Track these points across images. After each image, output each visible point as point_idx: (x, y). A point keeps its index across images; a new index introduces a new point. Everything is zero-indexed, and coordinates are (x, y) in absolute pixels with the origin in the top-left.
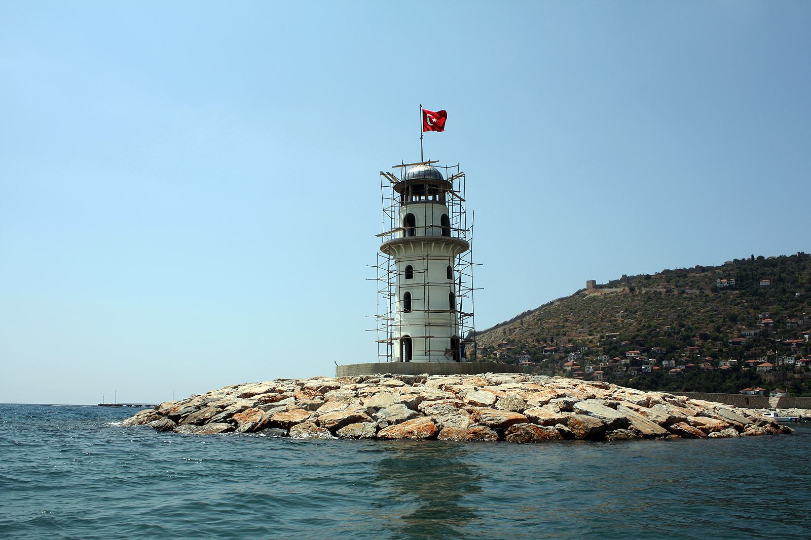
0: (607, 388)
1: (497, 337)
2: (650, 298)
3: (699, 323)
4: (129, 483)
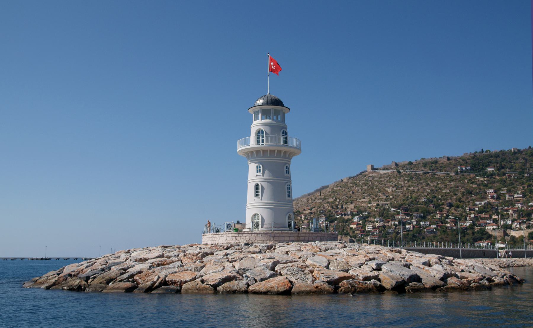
1: (302, 204)
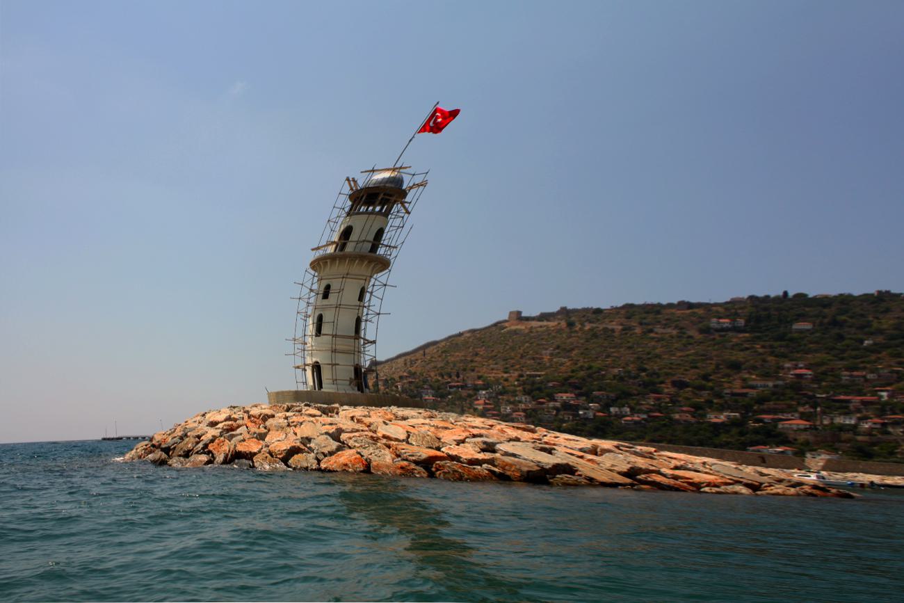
0: (533, 431)
2: (595, 336)
3: (671, 368)
4: (140, 525)
